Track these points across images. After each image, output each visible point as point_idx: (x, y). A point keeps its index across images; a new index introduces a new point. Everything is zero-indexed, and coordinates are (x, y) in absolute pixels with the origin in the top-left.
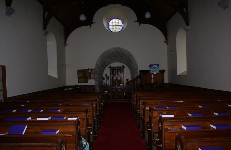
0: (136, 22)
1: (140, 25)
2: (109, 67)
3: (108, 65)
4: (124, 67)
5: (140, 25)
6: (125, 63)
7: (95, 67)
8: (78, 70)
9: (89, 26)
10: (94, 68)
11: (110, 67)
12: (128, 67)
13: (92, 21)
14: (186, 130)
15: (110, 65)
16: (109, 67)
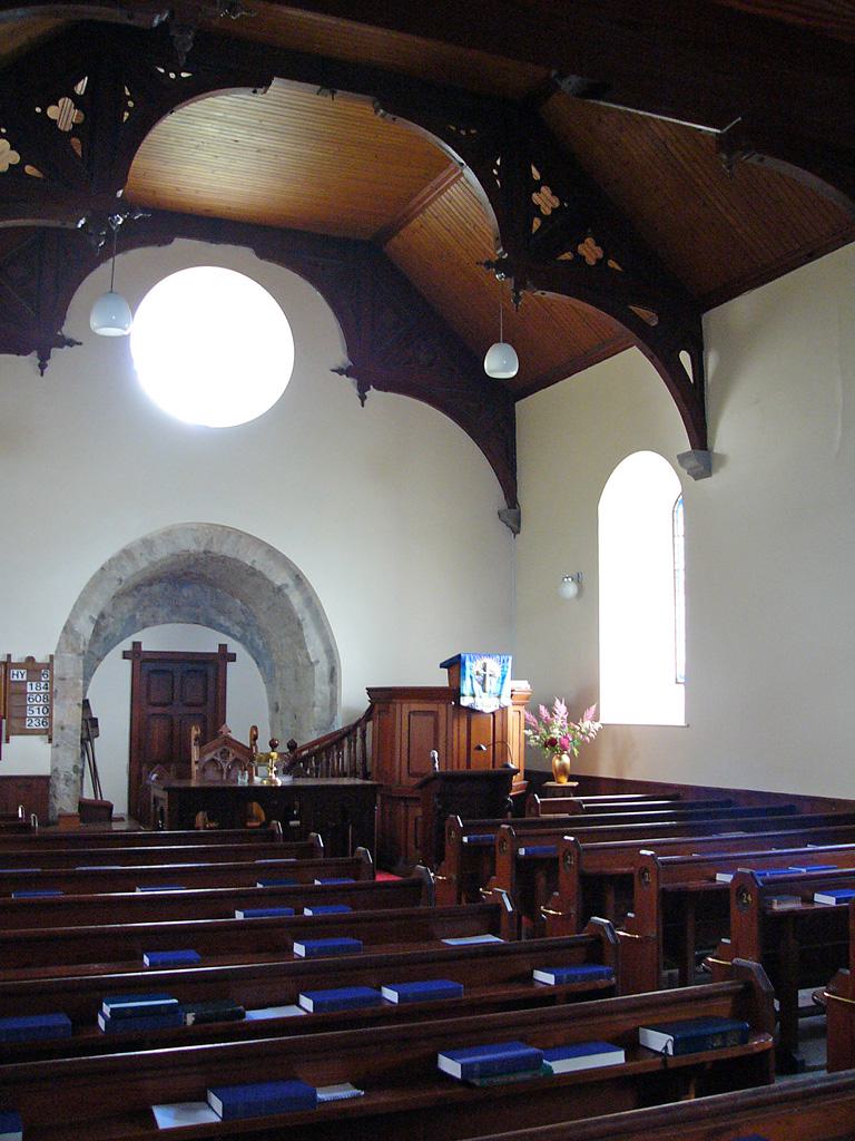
0: (42, 367)
1: (363, 398)
2: (125, 655)
4: (225, 656)
5: (363, 398)
6: (237, 630)
9: (33, 358)
11: (135, 654)
14: (440, 1056)
15: (136, 637)
16: (125, 655)
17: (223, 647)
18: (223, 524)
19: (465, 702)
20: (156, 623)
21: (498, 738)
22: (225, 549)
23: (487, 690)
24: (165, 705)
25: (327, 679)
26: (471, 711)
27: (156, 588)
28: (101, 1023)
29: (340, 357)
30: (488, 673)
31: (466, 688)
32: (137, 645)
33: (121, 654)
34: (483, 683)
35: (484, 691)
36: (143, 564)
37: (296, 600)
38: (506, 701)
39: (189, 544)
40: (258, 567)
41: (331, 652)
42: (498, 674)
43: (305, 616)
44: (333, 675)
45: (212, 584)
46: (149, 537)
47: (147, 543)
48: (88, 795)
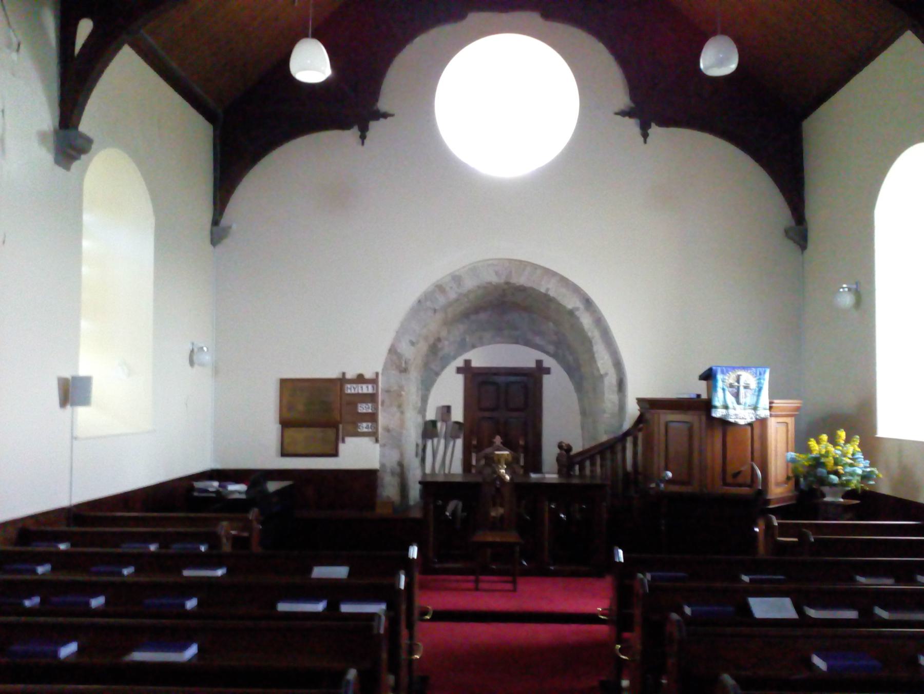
1: (645, 136)
2: (459, 370)
3: (455, 358)
5: (645, 136)
6: (551, 348)
7: (385, 368)
8: (284, 382)
10: (377, 374)
11: (466, 370)
12: (568, 373)
13: (376, 100)
15: (467, 356)
16: (459, 370)
17: (539, 363)
18: (547, 266)
19: (718, 413)
20: (482, 344)
21: (757, 445)
22: (521, 280)
23: (742, 400)
24: (493, 410)
25: (616, 389)
26: (724, 423)
27: (483, 316)
28: (663, 528)
29: (622, 99)
30: (742, 383)
31: (718, 401)
32: (467, 362)
33: (454, 370)
34: (737, 396)
35: (738, 403)
36: (453, 296)
37: (586, 321)
38: (763, 413)
39: (491, 278)
40: (552, 294)
41: (618, 365)
42: (753, 384)
43: (594, 334)
44: (621, 385)
45: (527, 309)
46: (457, 273)
47: (456, 279)
48: (447, 471)
